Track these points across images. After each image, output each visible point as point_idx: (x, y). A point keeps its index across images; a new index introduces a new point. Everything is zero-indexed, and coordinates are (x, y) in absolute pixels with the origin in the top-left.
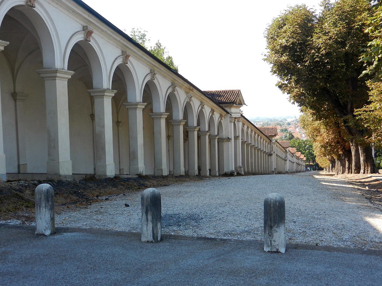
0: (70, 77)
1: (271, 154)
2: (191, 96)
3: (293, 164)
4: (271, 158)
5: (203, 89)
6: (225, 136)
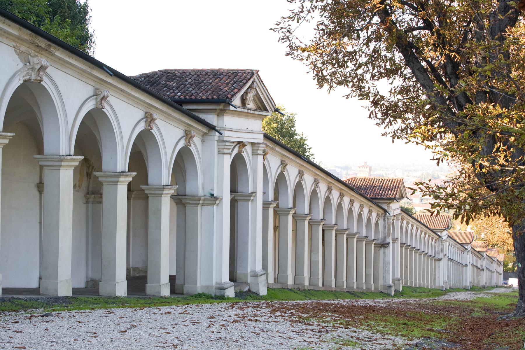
0: (77, 164)
1: (386, 242)
2: (39, 66)
3: (464, 268)
4: (384, 253)
5: (129, 72)
6: (203, 188)
